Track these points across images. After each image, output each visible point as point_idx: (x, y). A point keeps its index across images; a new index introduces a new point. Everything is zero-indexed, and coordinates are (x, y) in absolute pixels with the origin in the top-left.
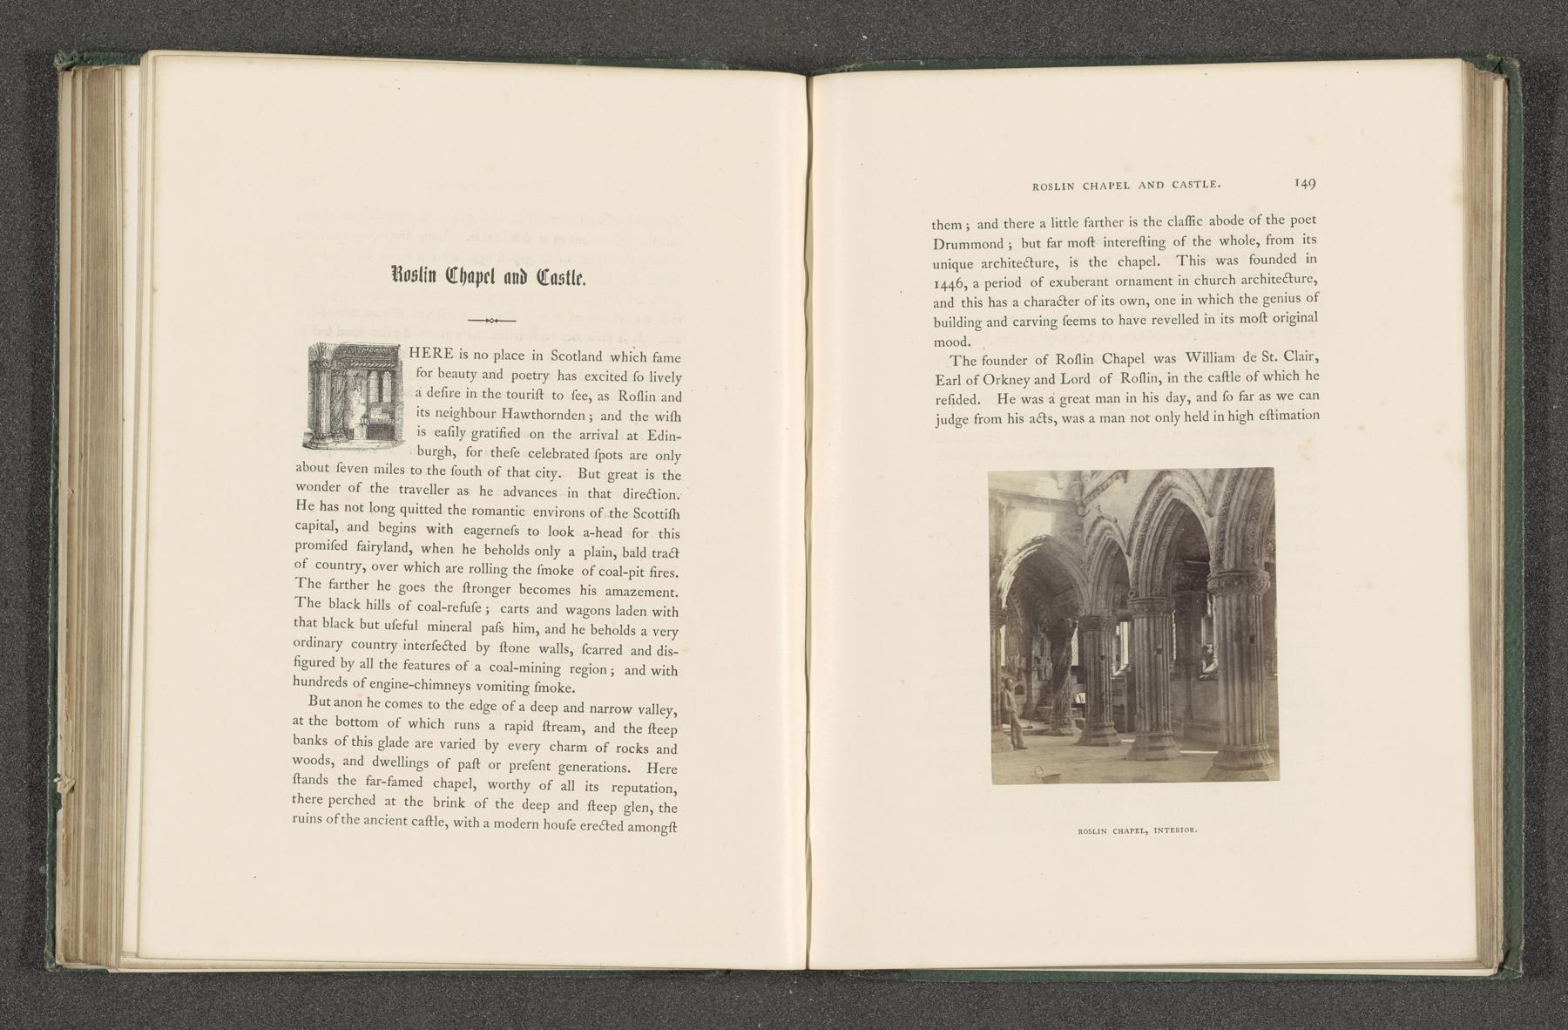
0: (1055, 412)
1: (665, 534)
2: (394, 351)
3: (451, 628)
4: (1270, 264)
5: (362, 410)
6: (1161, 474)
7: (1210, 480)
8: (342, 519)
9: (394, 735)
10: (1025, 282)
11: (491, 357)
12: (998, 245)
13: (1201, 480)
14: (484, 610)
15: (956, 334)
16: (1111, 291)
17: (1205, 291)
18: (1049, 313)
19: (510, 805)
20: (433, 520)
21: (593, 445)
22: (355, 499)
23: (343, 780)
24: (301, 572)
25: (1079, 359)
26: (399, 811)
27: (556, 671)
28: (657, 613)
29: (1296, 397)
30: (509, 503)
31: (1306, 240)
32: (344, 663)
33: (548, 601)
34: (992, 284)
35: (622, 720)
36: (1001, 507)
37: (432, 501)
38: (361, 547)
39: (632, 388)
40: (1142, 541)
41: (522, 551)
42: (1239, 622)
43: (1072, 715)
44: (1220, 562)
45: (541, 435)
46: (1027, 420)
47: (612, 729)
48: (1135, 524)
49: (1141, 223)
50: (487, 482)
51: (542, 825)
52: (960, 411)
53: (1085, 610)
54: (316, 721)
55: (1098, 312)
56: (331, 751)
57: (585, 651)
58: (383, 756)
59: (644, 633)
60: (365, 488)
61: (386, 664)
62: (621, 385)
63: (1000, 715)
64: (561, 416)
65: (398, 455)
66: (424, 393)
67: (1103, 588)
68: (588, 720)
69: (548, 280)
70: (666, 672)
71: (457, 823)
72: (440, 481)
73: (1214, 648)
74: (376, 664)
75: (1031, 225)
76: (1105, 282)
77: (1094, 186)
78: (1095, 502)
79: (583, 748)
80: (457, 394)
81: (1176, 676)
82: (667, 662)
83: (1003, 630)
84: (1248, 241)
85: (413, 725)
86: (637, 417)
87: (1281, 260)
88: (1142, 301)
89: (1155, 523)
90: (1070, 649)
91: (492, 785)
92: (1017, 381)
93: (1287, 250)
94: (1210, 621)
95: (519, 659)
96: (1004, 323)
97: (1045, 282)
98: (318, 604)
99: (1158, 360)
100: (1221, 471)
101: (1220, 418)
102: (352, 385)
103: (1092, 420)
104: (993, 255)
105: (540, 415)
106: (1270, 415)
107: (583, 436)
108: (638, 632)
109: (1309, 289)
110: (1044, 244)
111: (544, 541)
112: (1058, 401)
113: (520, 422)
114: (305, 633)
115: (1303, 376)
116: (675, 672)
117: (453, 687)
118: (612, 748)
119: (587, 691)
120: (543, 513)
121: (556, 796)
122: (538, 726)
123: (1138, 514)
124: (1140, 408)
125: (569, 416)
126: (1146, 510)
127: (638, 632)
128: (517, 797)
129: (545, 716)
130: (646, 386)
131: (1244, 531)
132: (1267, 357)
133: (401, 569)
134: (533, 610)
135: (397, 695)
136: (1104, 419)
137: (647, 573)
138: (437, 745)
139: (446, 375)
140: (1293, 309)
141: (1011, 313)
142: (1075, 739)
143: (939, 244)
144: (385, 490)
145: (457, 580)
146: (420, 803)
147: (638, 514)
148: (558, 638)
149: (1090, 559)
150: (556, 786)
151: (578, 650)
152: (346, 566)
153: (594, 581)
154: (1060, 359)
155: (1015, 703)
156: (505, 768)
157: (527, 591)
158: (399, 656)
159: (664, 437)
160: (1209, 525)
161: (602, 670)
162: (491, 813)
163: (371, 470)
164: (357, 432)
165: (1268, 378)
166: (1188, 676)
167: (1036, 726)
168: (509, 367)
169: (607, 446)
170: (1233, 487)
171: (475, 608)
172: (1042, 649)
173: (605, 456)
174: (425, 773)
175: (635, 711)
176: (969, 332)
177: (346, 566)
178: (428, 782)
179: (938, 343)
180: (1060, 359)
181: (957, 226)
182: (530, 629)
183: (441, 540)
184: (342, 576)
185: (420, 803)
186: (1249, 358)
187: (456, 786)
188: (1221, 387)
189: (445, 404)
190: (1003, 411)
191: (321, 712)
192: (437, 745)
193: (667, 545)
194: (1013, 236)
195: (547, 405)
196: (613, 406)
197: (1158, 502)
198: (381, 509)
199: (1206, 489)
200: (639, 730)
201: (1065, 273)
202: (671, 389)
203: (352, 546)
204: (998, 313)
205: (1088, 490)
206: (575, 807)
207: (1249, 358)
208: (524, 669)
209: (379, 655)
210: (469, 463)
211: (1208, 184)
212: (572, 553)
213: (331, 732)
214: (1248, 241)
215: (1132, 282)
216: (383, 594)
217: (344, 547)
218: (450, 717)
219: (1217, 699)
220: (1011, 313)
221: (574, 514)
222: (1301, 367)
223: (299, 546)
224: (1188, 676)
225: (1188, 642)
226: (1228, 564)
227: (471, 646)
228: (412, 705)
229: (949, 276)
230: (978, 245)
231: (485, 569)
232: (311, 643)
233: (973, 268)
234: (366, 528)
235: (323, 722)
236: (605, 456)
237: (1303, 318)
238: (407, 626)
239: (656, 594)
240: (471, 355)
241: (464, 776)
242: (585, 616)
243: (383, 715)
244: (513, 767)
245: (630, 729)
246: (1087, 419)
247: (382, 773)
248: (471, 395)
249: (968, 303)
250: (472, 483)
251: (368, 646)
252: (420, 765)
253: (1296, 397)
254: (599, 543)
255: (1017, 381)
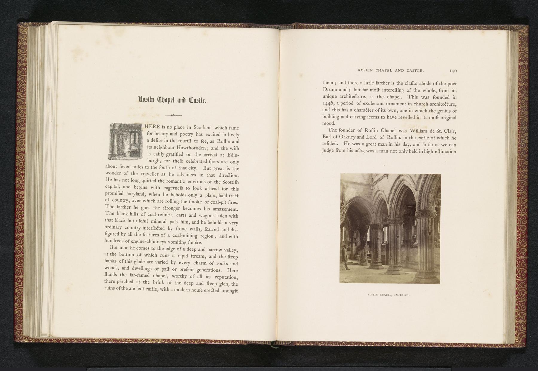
0: (364, 148)
1: (233, 189)
2: (140, 126)
3: (159, 222)
4: (440, 100)
5: (128, 146)
6: (400, 176)
7: (417, 178)
8: (122, 184)
9: (139, 259)
10: (355, 103)
11: (173, 128)
12: (346, 90)
13: (414, 178)
14: (170, 216)
15: (330, 120)
16: (385, 107)
17: (417, 108)
18: (363, 114)
19: (180, 283)
20: (153, 184)
21: (208, 158)
22: (126, 177)
23: (122, 275)
24: (107, 203)
25: (372, 130)
26: (141, 285)
27: (196, 237)
28: (231, 216)
29: (448, 145)
30: (180, 178)
31: (453, 91)
32: (122, 234)
33: (193, 212)
34: (343, 104)
35: (218, 254)
36: (344, 185)
37: (152, 178)
38: (128, 194)
39: (222, 138)
40: (393, 199)
41: (184, 195)
42: (425, 227)
43: (366, 259)
44: (419, 207)
45: (190, 155)
46: (354, 151)
47: (215, 257)
48: (391, 193)
49: (395, 83)
50: (171, 171)
51: (191, 290)
52: (331, 147)
53: (372, 222)
54: (113, 254)
55: (380, 114)
56: (118, 265)
57: (206, 230)
58: (136, 266)
59: (226, 223)
60: (129, 174)
61: (137, 235)
62: (218, 137)
63: (343, 259)
64: (197, 148)
65: (142, 162)
66: (150, 141)
67: (379, 215)
68: (207, 254)
69: (193, 101)
70: (234, 237)
71: (162, 290)
72: (156, 171)
73: (417, 237)
74: (133, 234)
75: (357, 83)
76: (382, 104)
77: (380, 70)
78: (377, 185)
79: (205, 263)
80: (161, 141)
81: (403, 246)
82: (234, 233)
83: (343, 228)
84: (432, 91)
85: (146, 255)
86: (224, 148)
87: (444, 98)
88: (395, 111)
89: (397, 193)
90: (367, 236)
91: (174, 276)
92: (351, 137)
93: (446, 94)
94: (415, 227)
95: (183, 233)
96: (347, 117)
97: (362, 103)
98: (113, 214)
99: (400, 131)
100: (421, 175)
101: (421, 152)
102: (126, 138)
103: (377, 152)
104: (344, 93)
105: (190, 148)
106: (439, 151)
107: (205, 155)
108: (224, 223)
109: (453, 108)
110: (361, 90)
111: (191, 192)
112: (365, 144)
113: (183, 150)
114: (109, 224)
115: (451, 138)
116: (237, 237)
117: (160, 242)
118: (215, 264)
119: (207, 243)
120: (191, 182)
121: (195, 280)
122: (189, 256)
123: (392, 189)
124: (394, 148)
125: (200, 148)
126: (394, 188)
127: (224, 223)
128: (182, 280)
129: (192, 252)
130: (227, 138)
131: (428, 196)
132: (439, 131)
133: (142, 201)
134: (188, 216)
135: (141, 245)
136: (381, 151)
137: (227, 203)
138: (154, 262)
139: (158, 134)
140: (448, 115)
141: (350, 114)
142: (368, 267)
143: (325, 89)
144: (136, 174)
145: (161, 205)
146: (148, 283)
147: (224, 182)
148: (196, 225)
149: (375, 205)
150: (196, 277)
151: (203, 229)
152: (123, 200)
153: (209, 205)
154: (366, 130)
155: (347, 254)
156: (178, 270)
157: (186, 209)
158: (141, 232)
159: (233, 155)
160: (416, 194)
161: (212, 237)
162: (173, 286)
163: (132, 167)
164: (127, 154)
165: (438, 138)
166: (408, 246)
167: (355, 262)
168: (179, 131)
169: (213, 159)
170: (425, 181)
171: (168, 215)
172: (357, 235)
173: (213, 162)
174: (150, 272)
175: (223, 250)
176: (335, 120)
177: (123, 200)
178: (151, 275)
179: (324, 124)
180: (366, 130)
181: (332, 83)
182: (187, 222)
183: (156, 191)
184: (122, 204)
185: (148, 283)
186: (432, 131)
187: (161, 276)
188: (422, 141)
189: (157, 144)
190: (346, 147)
191: (115, 251)
192: (154, 262)
193: (234, 193)
194: (351, 87)
195: (192, 144)
196: (215, 145)
197: (399, 185)
198: (135, 181)
199: (416, 181)
200: (224, 257)
201: (369, 100)
202: (235, 139)
203: (125, 194)
204: (345, 114)
205: (375, 180)
206: (202, 284)
207: (432, 131)
208: (184, 236)
209: (134, 231)
210: (166, 165)
211: (419, 70)
212: (201, 196)
213: (118, 258)
214: (432, 91)
215: (392, 104)
216: (136, 210)
217: (122, 194)
218: (159, 253)
219: (417, 254)
220: (350, 114)
221: (201, 182)
222: (450, 135)
223: (107, 194)
224: (408, 246)
225: (408, 234)
226: (422, 208)
227: (166, 228)
228: (146, 249)
229: (328, 100)
230: (339, 90)
231: (171, 201)
232: (111, 227)
233: (337, 97)
234: (129, 187)
235: (115, 255)
236: (213, 162)
237: (451, 118)
238: (144, 221)
239: (230, 210)
240: (166, 127)
241: (164, 273)
242: (206, 218)
243: (136, 252)
244: (181, 270)
245: (222, 257)
246: (375, 151)
247: (135, 272)
248: (166, 141)
249: (334, 110)
250: (166, 171)
251: (131, 228)
252: (149, 269)
253: (448, 145)
254: (211, 192)
255: (351, 137)
